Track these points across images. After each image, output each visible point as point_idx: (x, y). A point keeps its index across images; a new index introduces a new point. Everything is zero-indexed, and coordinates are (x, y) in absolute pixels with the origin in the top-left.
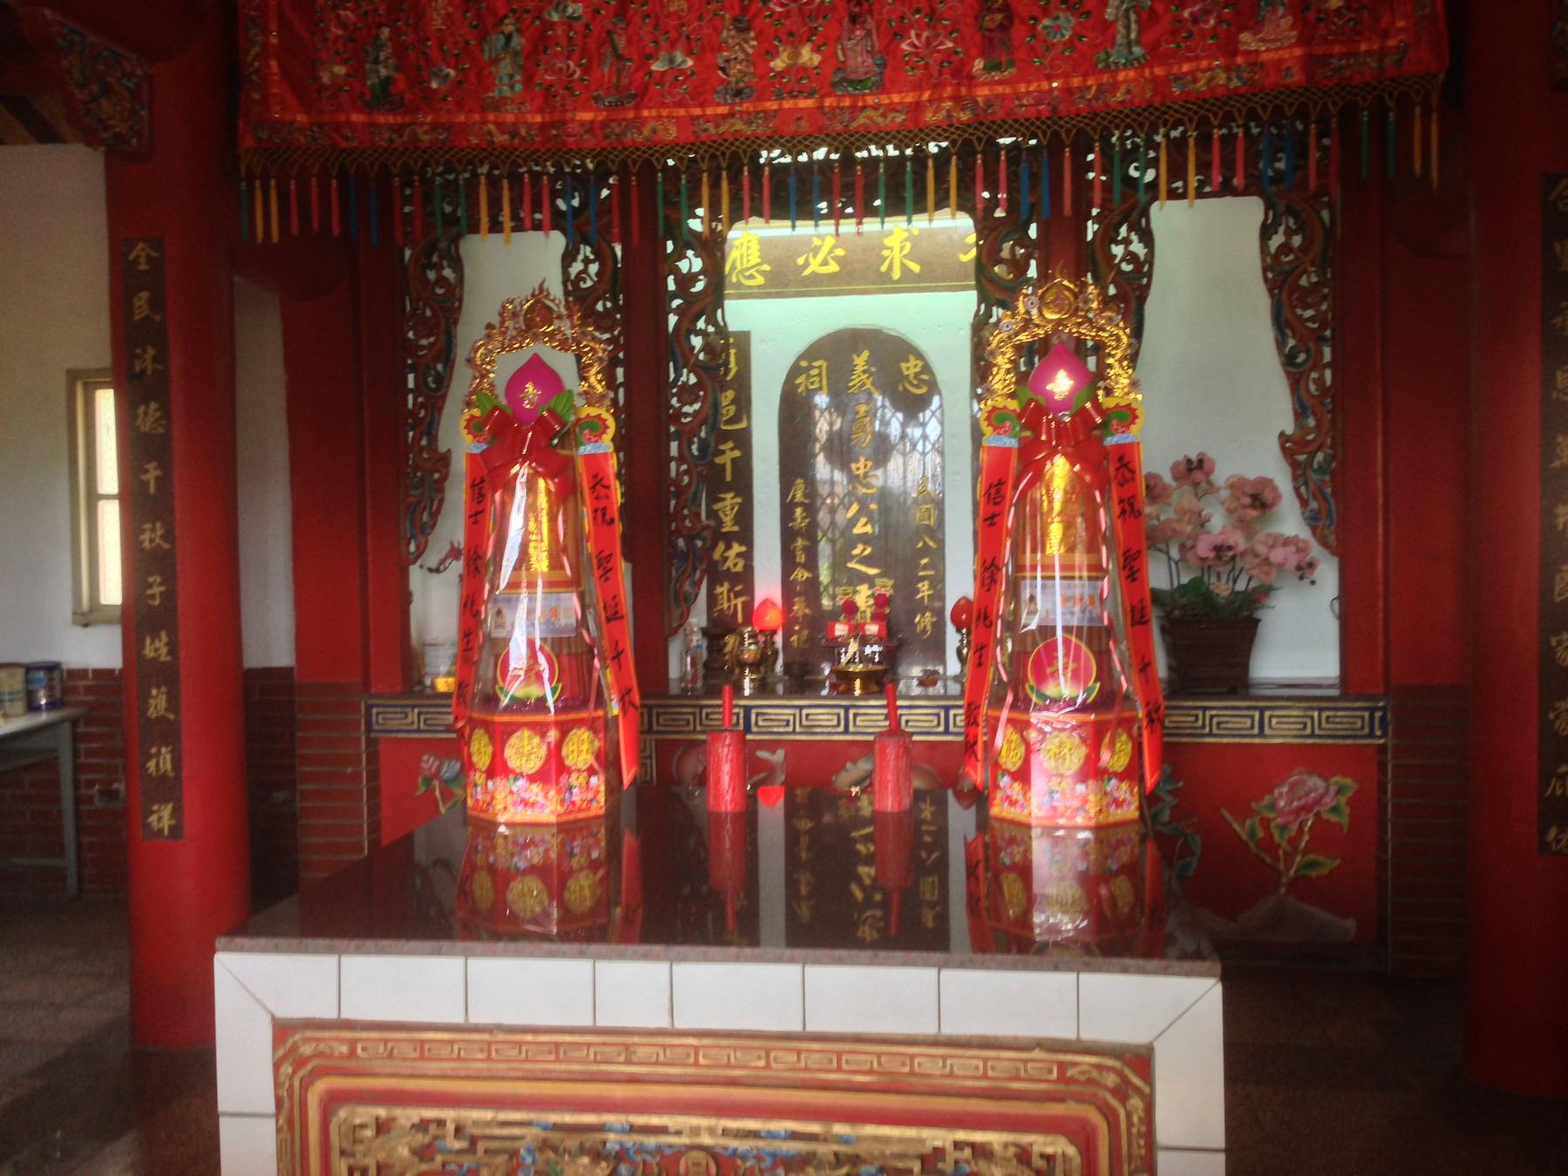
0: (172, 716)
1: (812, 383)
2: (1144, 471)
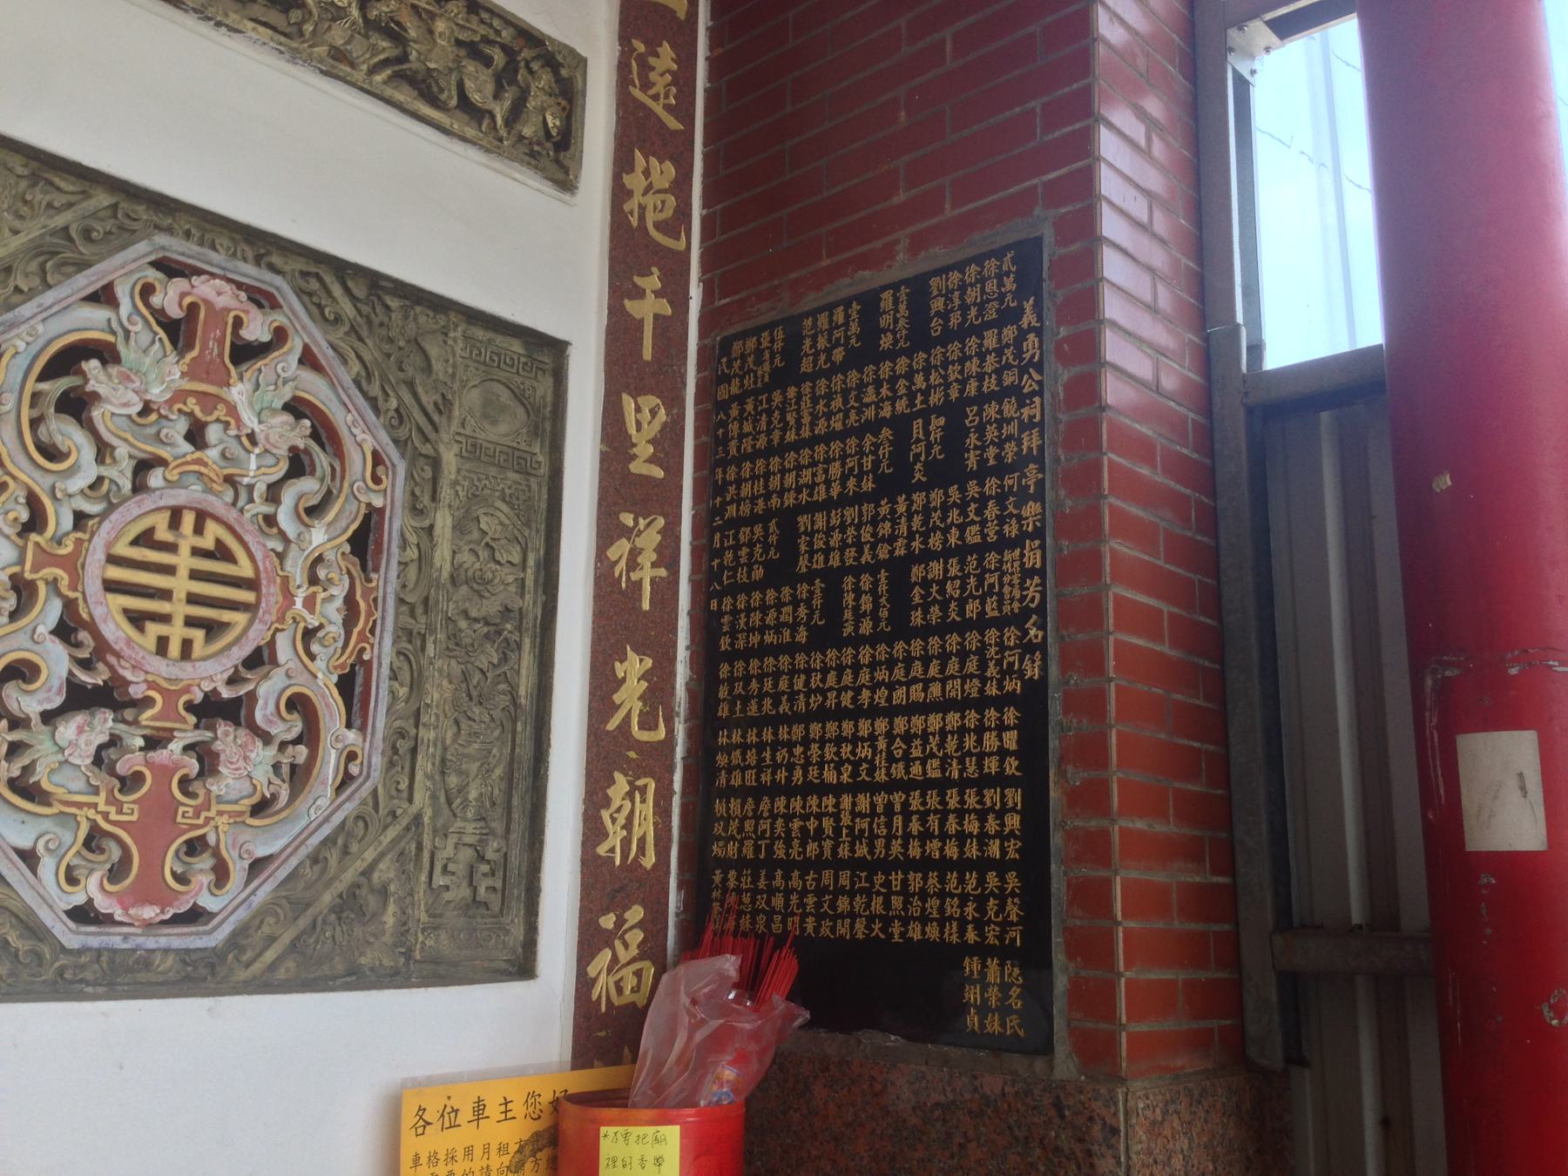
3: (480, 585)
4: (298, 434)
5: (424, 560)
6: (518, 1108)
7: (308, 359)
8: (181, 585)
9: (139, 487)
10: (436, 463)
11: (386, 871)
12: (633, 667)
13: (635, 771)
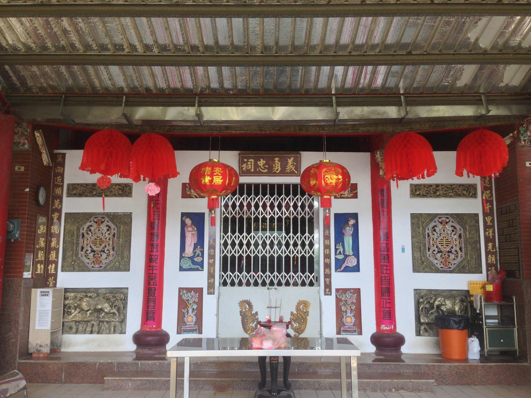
0: (56, 260)
1: (248, 167)
2: (482, 18)
3: (472, 238)
4: (453, 228)
5: (466, 237)
6: (481, 284)
7: (452, 222)
8: (445, 243)
9: (440, 236)
10: (466, 228)
11: (466, 264)
12: (490, 245)
13: (491, 255)
